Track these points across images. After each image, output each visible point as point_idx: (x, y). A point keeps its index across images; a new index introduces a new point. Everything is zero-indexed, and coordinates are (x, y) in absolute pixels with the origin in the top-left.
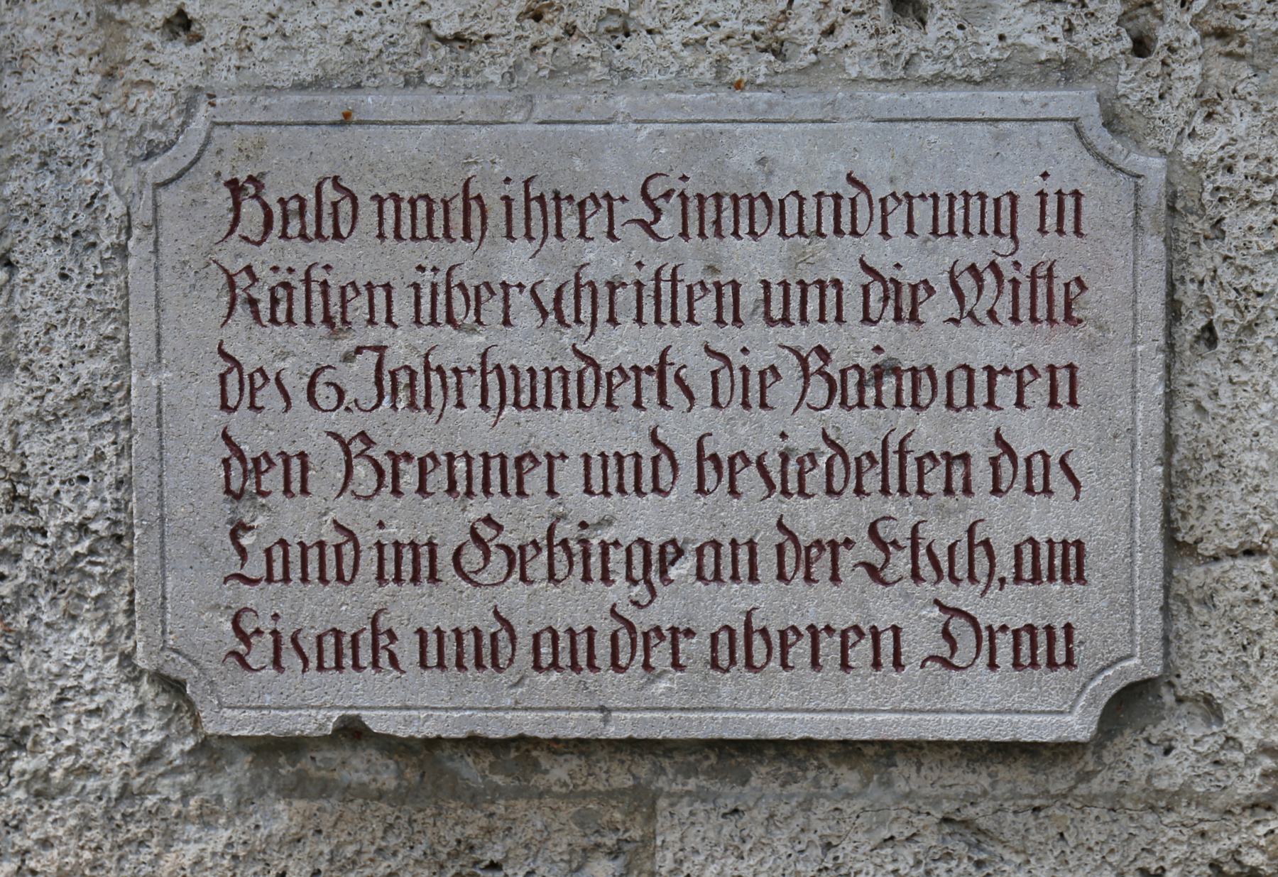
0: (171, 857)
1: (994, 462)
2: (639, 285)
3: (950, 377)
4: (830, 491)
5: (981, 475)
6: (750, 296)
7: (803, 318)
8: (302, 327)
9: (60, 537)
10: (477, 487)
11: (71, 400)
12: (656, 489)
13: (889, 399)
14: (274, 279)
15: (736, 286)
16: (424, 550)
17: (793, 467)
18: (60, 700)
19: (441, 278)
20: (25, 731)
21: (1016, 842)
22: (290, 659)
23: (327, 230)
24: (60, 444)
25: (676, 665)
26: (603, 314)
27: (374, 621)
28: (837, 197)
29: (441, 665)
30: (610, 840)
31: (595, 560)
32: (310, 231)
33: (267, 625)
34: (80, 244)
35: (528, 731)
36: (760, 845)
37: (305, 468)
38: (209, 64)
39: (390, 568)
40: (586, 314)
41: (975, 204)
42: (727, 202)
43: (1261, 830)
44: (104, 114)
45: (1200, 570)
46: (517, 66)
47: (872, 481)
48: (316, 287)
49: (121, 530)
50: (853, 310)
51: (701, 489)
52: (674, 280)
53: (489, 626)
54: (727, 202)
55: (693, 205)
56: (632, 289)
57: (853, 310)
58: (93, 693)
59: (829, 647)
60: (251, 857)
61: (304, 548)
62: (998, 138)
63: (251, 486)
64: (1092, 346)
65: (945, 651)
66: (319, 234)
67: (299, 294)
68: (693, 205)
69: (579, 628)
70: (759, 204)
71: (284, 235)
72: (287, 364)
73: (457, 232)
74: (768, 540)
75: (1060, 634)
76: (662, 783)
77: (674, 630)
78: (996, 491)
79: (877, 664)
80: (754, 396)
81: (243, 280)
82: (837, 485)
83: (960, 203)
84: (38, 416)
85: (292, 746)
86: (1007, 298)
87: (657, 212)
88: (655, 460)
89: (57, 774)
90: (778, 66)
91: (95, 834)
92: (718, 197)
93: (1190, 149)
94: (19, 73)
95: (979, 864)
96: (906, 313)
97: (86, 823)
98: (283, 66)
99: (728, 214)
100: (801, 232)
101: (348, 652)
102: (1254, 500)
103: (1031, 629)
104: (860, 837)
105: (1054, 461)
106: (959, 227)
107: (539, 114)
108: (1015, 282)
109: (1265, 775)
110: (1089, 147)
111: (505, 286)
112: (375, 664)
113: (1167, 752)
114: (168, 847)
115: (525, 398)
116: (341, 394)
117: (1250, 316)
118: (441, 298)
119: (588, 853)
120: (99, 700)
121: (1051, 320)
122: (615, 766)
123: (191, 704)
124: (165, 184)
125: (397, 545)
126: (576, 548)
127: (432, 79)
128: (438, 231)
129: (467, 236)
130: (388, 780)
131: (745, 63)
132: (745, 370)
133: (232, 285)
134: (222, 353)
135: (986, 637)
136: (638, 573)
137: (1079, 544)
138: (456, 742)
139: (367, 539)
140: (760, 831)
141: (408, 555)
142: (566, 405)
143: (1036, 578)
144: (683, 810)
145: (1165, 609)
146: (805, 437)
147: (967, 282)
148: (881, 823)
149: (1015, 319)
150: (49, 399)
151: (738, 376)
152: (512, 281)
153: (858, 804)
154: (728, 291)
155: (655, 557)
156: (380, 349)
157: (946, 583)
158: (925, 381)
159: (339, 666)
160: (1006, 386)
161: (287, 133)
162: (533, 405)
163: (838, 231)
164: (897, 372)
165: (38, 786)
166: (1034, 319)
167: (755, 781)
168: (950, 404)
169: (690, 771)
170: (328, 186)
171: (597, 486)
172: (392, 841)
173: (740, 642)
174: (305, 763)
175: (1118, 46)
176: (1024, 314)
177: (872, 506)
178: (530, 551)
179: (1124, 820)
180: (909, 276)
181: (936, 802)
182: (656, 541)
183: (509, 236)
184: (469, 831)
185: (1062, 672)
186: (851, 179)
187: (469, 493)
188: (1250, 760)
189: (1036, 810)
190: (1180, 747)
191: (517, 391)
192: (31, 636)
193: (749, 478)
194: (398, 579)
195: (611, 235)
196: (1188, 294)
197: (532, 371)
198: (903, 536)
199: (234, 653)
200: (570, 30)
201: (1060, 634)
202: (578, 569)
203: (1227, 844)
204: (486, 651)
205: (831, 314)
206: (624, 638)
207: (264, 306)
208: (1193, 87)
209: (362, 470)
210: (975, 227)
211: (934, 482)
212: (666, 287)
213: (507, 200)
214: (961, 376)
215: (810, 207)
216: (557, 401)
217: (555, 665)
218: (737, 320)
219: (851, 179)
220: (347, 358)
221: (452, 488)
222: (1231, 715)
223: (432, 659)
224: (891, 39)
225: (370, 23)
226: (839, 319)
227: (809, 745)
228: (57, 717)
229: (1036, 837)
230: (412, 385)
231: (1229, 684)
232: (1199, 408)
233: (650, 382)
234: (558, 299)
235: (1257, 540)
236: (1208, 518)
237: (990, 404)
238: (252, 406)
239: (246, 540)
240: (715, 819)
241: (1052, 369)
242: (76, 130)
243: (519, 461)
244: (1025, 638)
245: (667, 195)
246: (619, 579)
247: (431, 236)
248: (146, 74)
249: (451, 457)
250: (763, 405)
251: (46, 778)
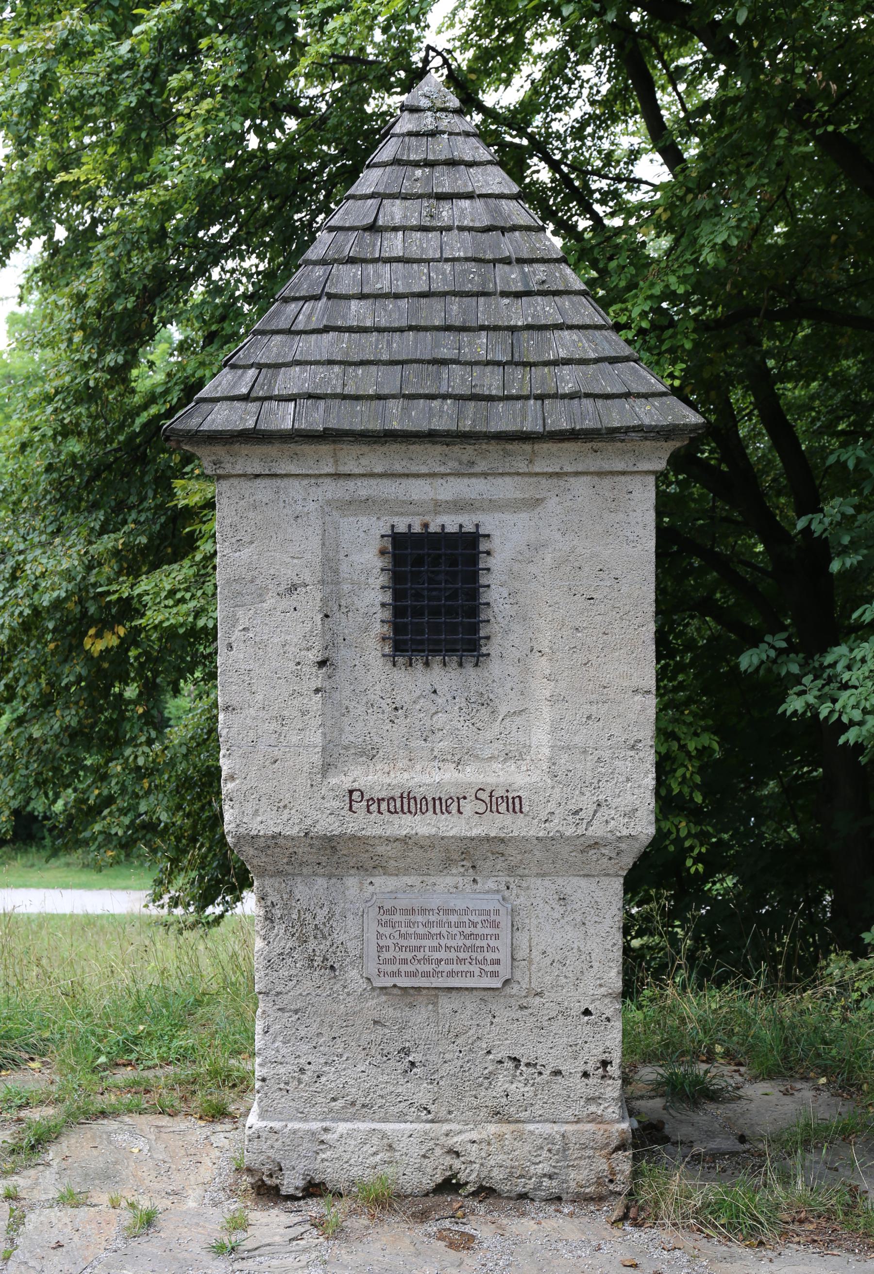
85: (385, 988)
135: (486, 973)
146: (460, 944)
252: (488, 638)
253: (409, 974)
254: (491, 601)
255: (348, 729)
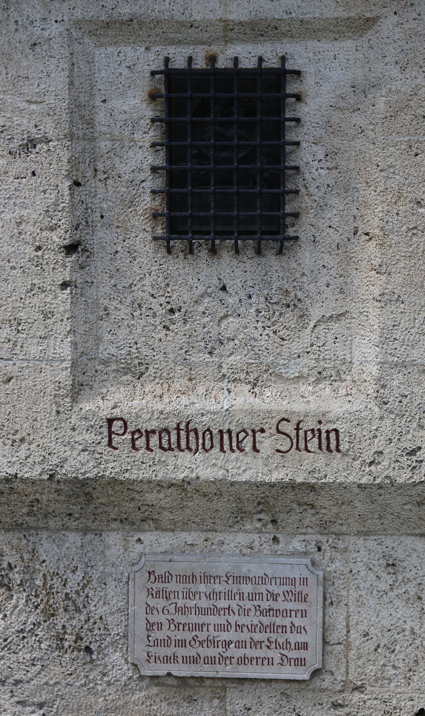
0: (133, 697)
1: (291, 627)
2: (225, 593)
3: (283, 611)
4: (260, 632)
5: (289, 630)
6: (246, 595)
7: (256, 600)
8: (161, 599)
9: (114, 636)
10: (194, 630)
11: (117, 610)
12: (228, 631)
13: (271, 615)
14: (156, 590)
15: (243, 593)
16: (184, 641)
17: (253, 627)
18: (113, 667)
19: (188, 590)
20: (106, 673)
21: (295, 697)
22: (158, 661)
23: (167, 581)
24: (114, 618)
25: (231, 664)
26: (218, 598)
27: (174, 654)
28: (262, 577)
29: (186, 663)
30: (218, 696)
31: (216, 644)
32: (163, 581)
33: (154, 655)
34: (119, 581)
35: (203, 675)
36: (246, 697)
37: (161, 625)
38: (144, 548)
39: (177, 644)
40: (215, 598)
41: (288, 579)
42: (241, 578)
43: (341, 696)
44: (124, 557)
45: (330, 647)
46: (202, 550)
47: (268, 630)
48: (164, 592)
49: (126, 635)
50: (265, 598)
51: (236, 631)
52: (231, 592)
53: (196, 656)
54: (241, 578)
55: (235, 578)
56: (224, 593)
57: (265, 598)
58: (119, 666)
59: (260, 661)
60: (149, 698)
61: (161, 640)
62: (292, 567)
63: (151, 628)
64: (309, 606)
65: (281, 662)
66: (165, 582)
67: (161, 593)
68: (235, 578)
69: (213, 656)
70: (248, 578)
71: (158, 582)
72: (158, 606)
73: (191, 582)
74: (248, 641)
75: (303, 660)
76: (228, 685)
77: (231, 657)
78: (291, 632)
79: (269, 664)
80: (246, 614)
81: (150, 590)
82: (262, 631)
83: (285, 579)
84: (110, 613)
85: (157, 677)
86: (294, 597)
87: (229, 579)
88: (227, 625)
89: (112, 681)
90: (252, 551)
91: (119, 693)
92: (240, 577)
93: (328, 569)
94: (108, 549)
95: (288, 702)
96: (275, 599)
97: (117, 690)
98: (159, 549)
99: (242, 580)
100: (255, 583)
101: (169, 660)
102: (340, 634)
103: (297, 658)
104: (265, 696)
105: (302, 627)
106: (285, 583)
107: (207, 560)
108: (295, 594)
109: (342, 686)
110: (309, 570)
111: (200, 592)
112: (174, 662)
113: (324, 681)
114: (133, 695)
115: (203, 613)
116: (168, 611)
117: (339, 600)
118: (188, 594)
119: (213, 698)
120: (120, 667)
121: (302, 601)
122: (219, 682)
123: (138, 669)
124: (136, 572)
125: (179, 640)
126: (212, 641)
127: (186, 552)
128: (187, 581)
129: (193, 583)
130: (175, 683)
131: (245, 551)
132: (244, 609)
133: (148, 591)
134: (146, 603)
135: (289, 660)
136: (224, 646)
137: (307, 643)
138: (188, 677)
139: (173, 639)
140: (246, 695)
141: (180, 642)
142: (211, 614)
143: (299, 649)
144: (232, 690)
145: (323, 655)
146: (256, 621)
147: (286, 594)
148: (269, 693)
149: (295, 601)
150: (112, 610)
151: (243, 610)
152: (201, 591)
153: (265, 690)
154: (242, 594)
155: (227, 643)
156: (176, 603)
157: (282, 649)
158: (278, 612)
159: (167, 663)
160: (293, 613)
161: (159, 563)
162: (205, 614)
163: (262, 584)
164: (273, 610)
165: (108, 683)
166: (298, 601)
167: (245, 685)
168: (283, 616)
169: (233, 683)
170: (167, 573)
171: (216, 629)
172: (176, 695)
173: (243, 660)
174: (159, 680)
175: (315, 550)
176: (297, 600)
177: (268, 635)
178: (204, 642)
179: (315, 694)
180: (275, 592)
181: (280, 690)
182: (227, 640)
183: (201, 583)
184: (191, 693)
185: (303, 667)
186: (265, 574)
187: (192, 631)
188: (339, 683)
189: (299, 691)
190: (326, 680)
191: (202, 612)
192: (108, 655)
193: (245, 629)
194: (179, 646)
195: (220, 583)
196: (328, 596)
197: (205, 608)
198: (274, 640)
199: (147, 660)
200: (213, 544)
201: (303, 660)
202: (213, 645)
203: (335, 699)
204: (195, 660)
205: (261, 599)
206: (221, 658)
207: (154, 595)
208: (329, 557)
209: (172, 626)
210: (288, 584)
211: (280, 630)
212: (230, 593)
213: (201, 576)
214: (285, 611)
215: (257, 579)
216: (209, 614)
217: (208, 663)
218: (243, 600)
219: (265, 574)
220: (170, 605)
221: (189, 630)
222: (336, 674)
223: (185, 661)
224: (273, 547)
225: (175, 541)
226: (262, 600)
227: (256, 679)
228: (112, 670)
229: (299, 697)
230: (182, 610)
231: (335, 669)
232: (330, 617)
233: (227, 611)
234: (210, 595)
235: (341, 641)
236: (331, 637)
237: (290, 616)
238: (152, 613)
239: (150, 639)
240: (238, 692)
241: (302, 610)
242: (119, 560)
243: (202, 625)
244: (296, 660)
245: (230, 576)
246: (220, 647)
247: (186, 582)
248: (133, 550)
249: (189, 624)
250: (248, 615)
251: (110, 682)
252: (296, 215)
253: (187, 660)
254: (301, 164)
255: (107, 337)
